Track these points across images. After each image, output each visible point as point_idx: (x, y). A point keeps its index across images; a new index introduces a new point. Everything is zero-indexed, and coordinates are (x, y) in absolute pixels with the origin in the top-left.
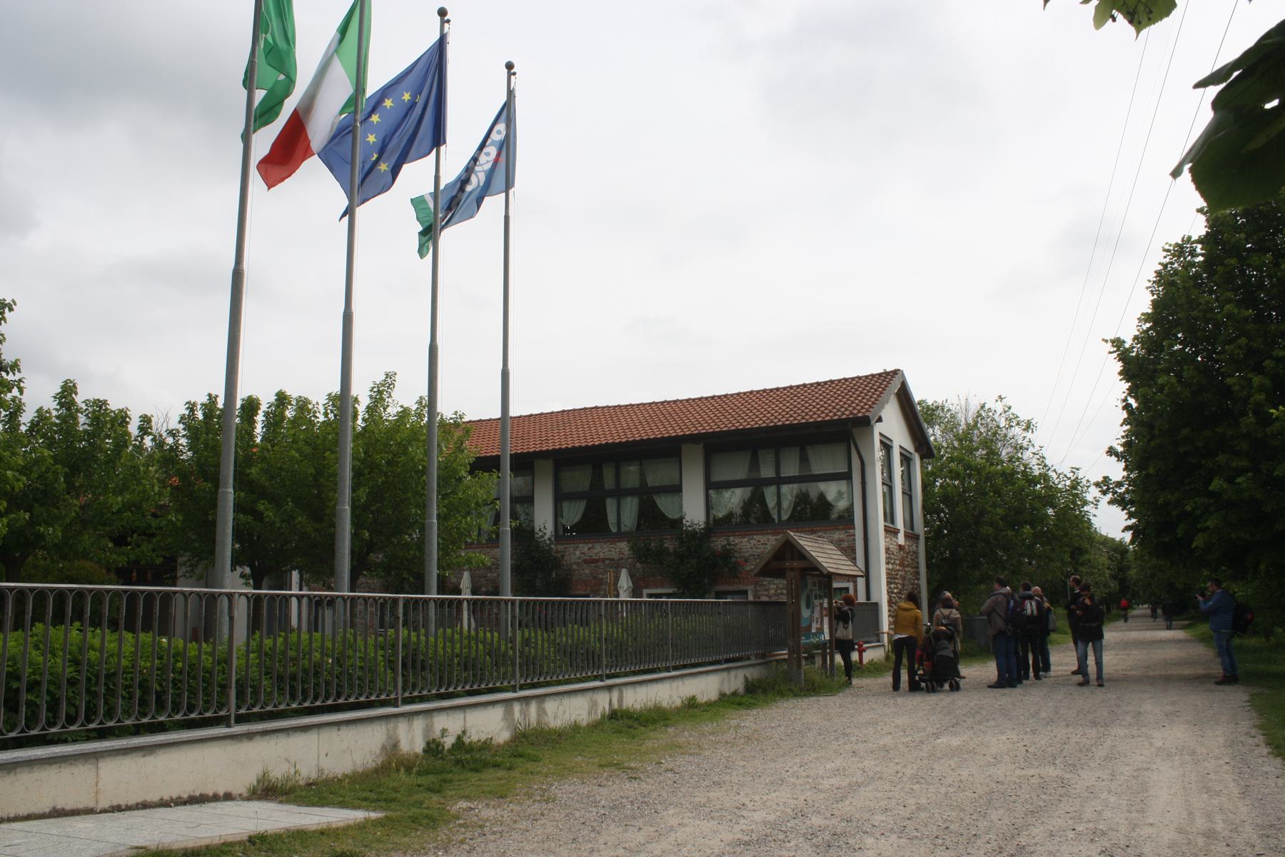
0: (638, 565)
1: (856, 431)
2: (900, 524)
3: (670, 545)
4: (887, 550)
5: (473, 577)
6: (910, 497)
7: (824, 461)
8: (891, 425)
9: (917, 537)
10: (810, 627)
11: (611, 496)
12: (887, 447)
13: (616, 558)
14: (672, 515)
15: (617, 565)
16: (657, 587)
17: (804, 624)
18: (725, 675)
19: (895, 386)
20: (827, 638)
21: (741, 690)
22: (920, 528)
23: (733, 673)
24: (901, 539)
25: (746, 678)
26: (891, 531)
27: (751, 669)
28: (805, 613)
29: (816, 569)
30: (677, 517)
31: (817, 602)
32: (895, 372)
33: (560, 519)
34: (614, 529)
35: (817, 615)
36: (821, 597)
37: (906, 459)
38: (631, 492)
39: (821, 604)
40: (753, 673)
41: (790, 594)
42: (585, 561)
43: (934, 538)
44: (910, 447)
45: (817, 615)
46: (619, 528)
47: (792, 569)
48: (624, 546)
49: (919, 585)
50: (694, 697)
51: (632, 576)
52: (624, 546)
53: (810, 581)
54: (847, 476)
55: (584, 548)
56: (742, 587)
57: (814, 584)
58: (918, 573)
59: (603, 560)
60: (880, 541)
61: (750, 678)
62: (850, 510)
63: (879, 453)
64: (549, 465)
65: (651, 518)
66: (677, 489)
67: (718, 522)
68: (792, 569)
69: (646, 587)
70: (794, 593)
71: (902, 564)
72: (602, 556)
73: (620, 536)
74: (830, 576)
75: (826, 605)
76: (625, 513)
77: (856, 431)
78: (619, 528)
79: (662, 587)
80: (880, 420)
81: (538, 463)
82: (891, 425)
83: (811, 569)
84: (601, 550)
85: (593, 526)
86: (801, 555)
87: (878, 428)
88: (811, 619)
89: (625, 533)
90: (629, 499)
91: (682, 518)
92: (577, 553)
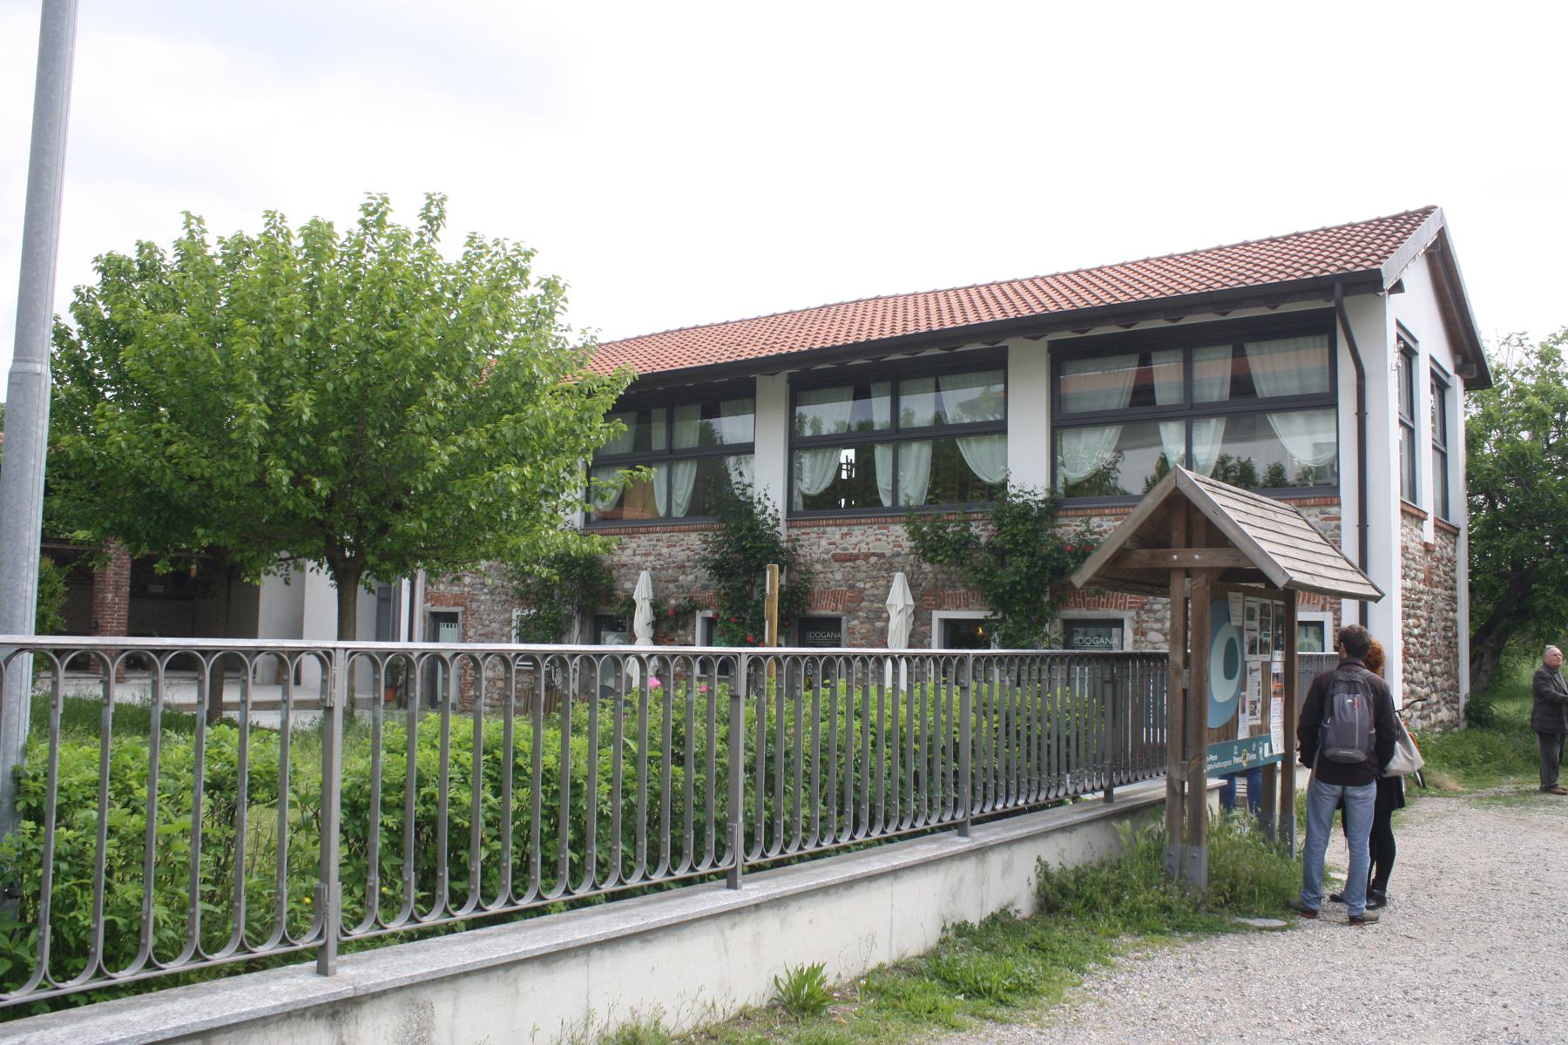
0: (927, 567)
1: (1350, 303)
2: (1428, 500)
3: (981, 531)
4: (1405, 549)
5: (655, 581)
6: (1444, 456)
7: (1277, 368)
8: (1413, 308)
9: (1453, 532)
10: (1231, 728)
11: (882, 442)
12: (1408, 354)
13: (888, 553)
14: (988, 475)
15: (888, 565)
16: (958, 607)
17: (1214, 721)
18: (968, 868)
19: (1425, 235)
20: (1279, 749)
21: (1024, 906)
22: (1459, 515)
23: (996, 860)
24: (1428, 533)
25: (1043, 867)
26: (1413, 515)
27: (1062, 840)
28: (1220, 689)
29: (1259, 575)
30: (998, 479)
31: (1255, 661)
32: (1427, 211)
33: (797, 483)
34: (887, 502)
35: (1253, 692)
36: (1264, 648)
37: (1440, 386)
38: (918, 435)
39: (1266, 666)
40: (1068, 853)
41: (1178, 635)
42: (836, 558)
43: (1485, 536)
44: (1447, 364)
45: (1253, 692)
46: (895, 493)
47: (1188, 572)
48: (899, 531)
49: (1454, 622)
50: (815, 971)
51: (913, 586)
52: (899, 531)
53: (1237, 604)
54: (1326, 402)
55: (834, 533)
56: (1113, 613)
57: (1250, 614)
58: (1454, 599)
59: (867, 556)
60: (1391, 533)
61: (1054, 866)
62: (1333, 469)
63: (1393, 357)
64: (773, 391)
65: (954, 482)
66: (999, 429)
67: (1074, 490)
68: (1188, 572)
69: (939, 607)
70: (1193, 636)
71: (1428, 581)
72: (864, 549)
73: (897, 512)
74: (1291, 594)
75: (1277, 668)
76: (911, 474)
77: (1350, 303)
78: (895, 493)
79: (967, 607)
80: (1398, 287)
81: (762, 382)
82: (1413, 308)
83: (1242, 574)
84: (865, 538)
85: (855, 496)
86: (1213, 534)
87: (1395, 307)
88: (1236, 705)
89: (908, 508)
90: (915, 446)
91: (1003, 485)
92: (821, 543)
